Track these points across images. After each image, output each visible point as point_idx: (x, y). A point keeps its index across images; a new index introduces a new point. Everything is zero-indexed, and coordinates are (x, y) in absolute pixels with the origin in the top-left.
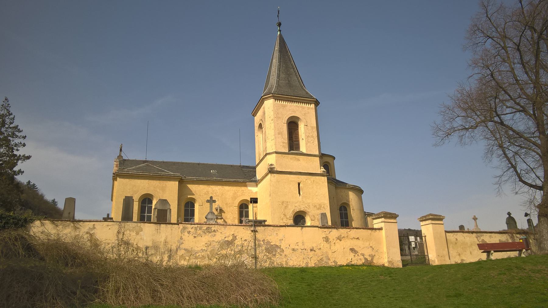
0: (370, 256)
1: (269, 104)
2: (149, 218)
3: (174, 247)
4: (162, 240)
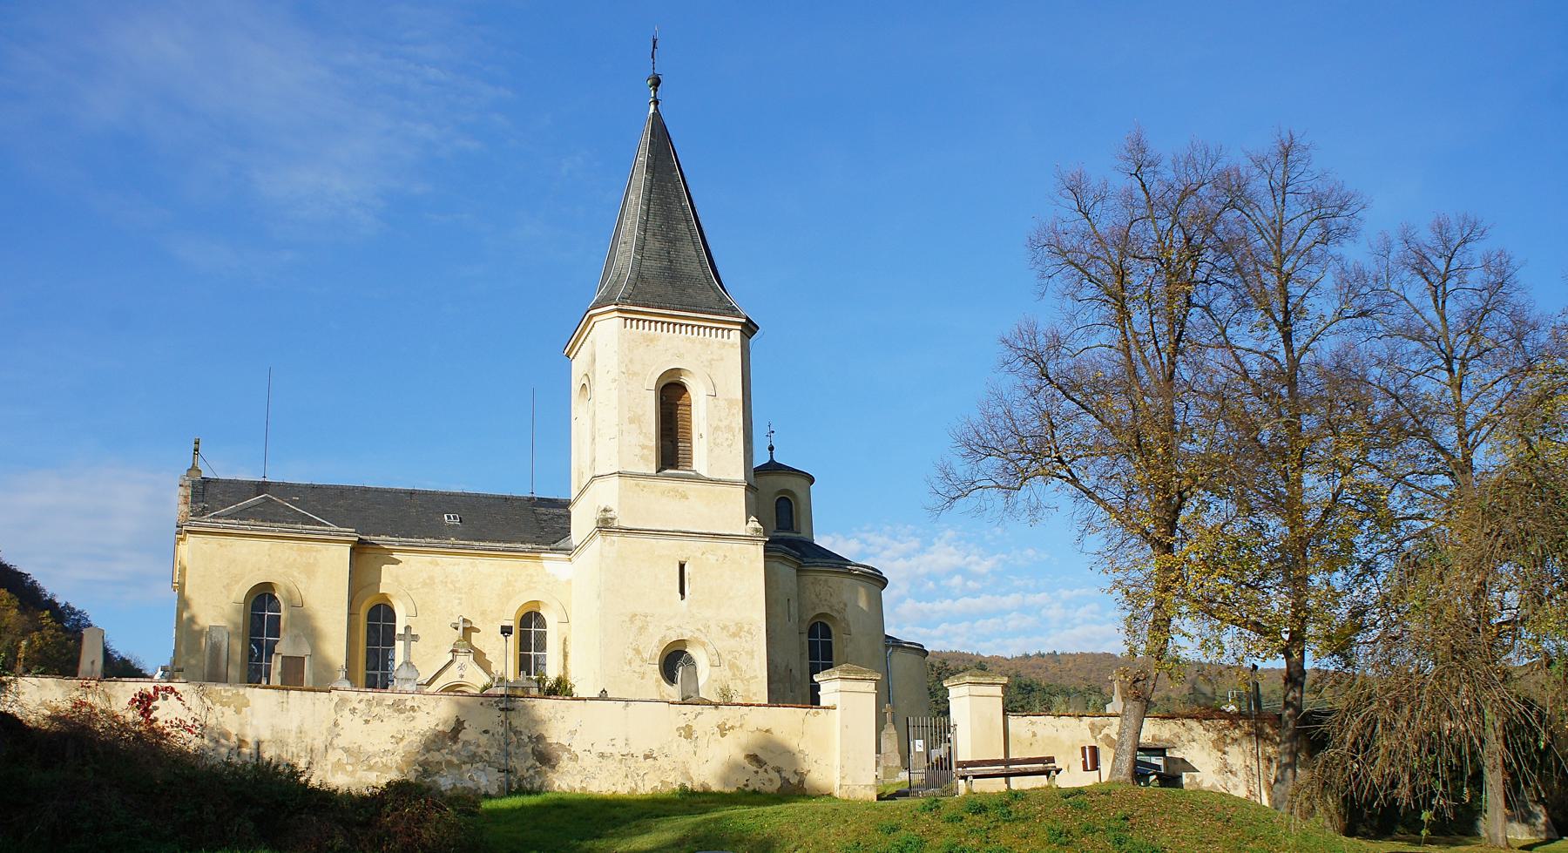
1: (608, 330)
3: (319, 744)
4: (294, 726)
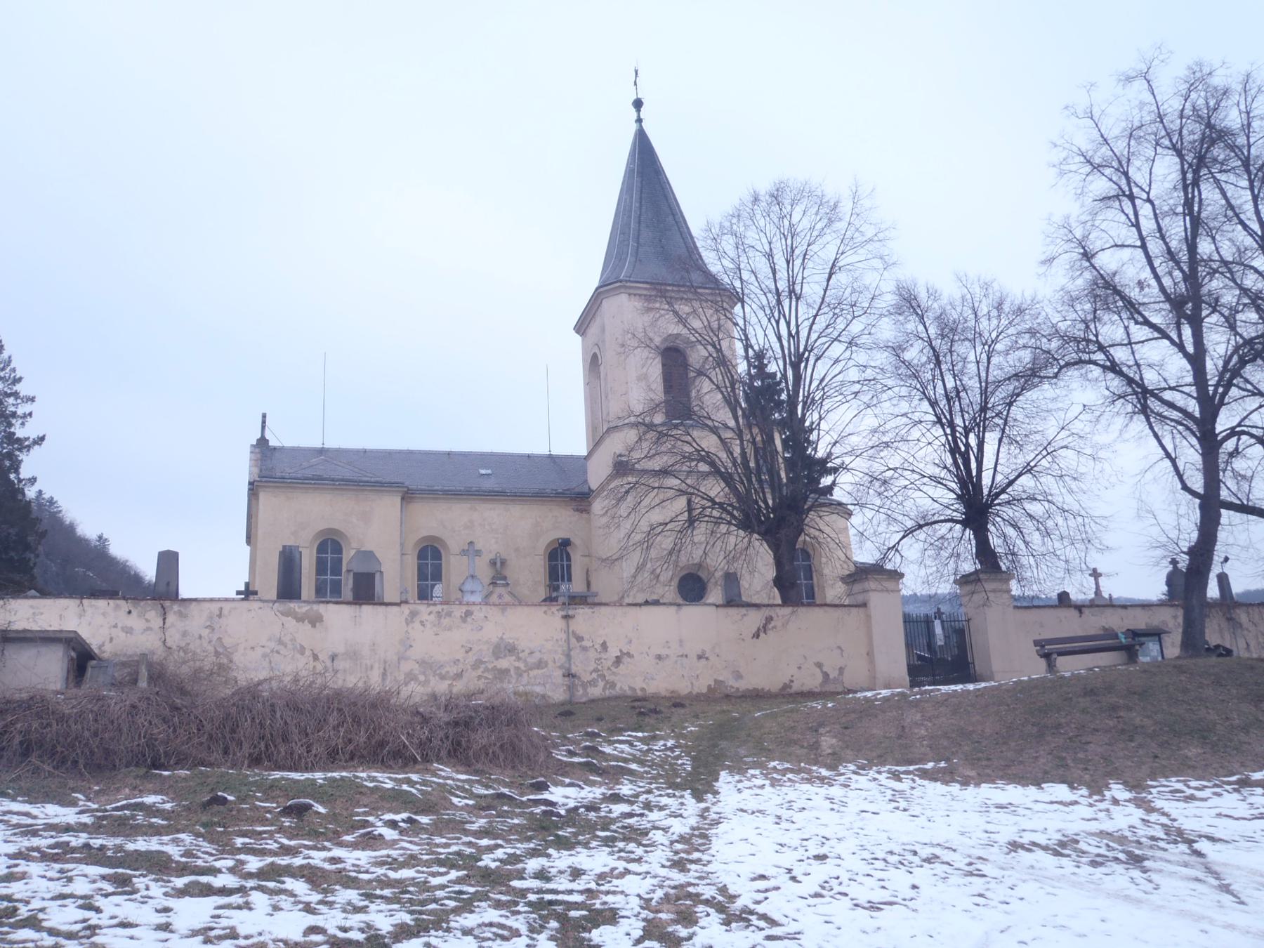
0: (270, 639)
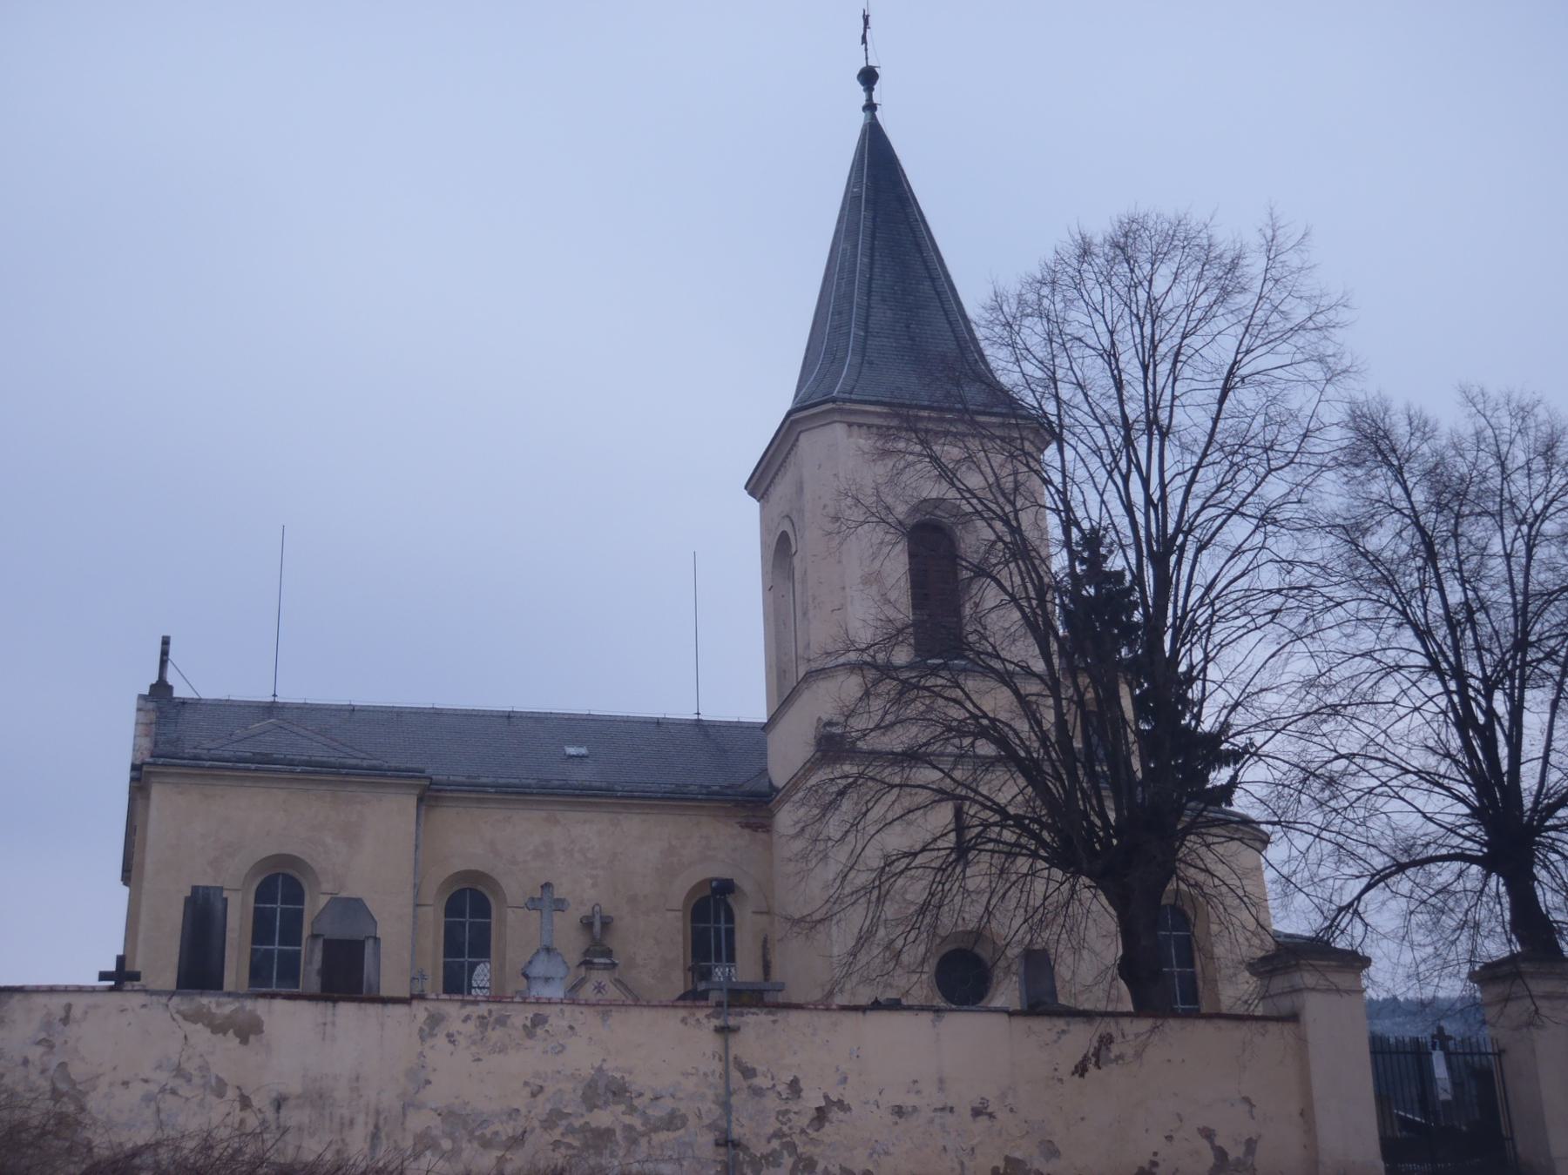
2: (290, 970)
